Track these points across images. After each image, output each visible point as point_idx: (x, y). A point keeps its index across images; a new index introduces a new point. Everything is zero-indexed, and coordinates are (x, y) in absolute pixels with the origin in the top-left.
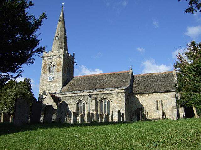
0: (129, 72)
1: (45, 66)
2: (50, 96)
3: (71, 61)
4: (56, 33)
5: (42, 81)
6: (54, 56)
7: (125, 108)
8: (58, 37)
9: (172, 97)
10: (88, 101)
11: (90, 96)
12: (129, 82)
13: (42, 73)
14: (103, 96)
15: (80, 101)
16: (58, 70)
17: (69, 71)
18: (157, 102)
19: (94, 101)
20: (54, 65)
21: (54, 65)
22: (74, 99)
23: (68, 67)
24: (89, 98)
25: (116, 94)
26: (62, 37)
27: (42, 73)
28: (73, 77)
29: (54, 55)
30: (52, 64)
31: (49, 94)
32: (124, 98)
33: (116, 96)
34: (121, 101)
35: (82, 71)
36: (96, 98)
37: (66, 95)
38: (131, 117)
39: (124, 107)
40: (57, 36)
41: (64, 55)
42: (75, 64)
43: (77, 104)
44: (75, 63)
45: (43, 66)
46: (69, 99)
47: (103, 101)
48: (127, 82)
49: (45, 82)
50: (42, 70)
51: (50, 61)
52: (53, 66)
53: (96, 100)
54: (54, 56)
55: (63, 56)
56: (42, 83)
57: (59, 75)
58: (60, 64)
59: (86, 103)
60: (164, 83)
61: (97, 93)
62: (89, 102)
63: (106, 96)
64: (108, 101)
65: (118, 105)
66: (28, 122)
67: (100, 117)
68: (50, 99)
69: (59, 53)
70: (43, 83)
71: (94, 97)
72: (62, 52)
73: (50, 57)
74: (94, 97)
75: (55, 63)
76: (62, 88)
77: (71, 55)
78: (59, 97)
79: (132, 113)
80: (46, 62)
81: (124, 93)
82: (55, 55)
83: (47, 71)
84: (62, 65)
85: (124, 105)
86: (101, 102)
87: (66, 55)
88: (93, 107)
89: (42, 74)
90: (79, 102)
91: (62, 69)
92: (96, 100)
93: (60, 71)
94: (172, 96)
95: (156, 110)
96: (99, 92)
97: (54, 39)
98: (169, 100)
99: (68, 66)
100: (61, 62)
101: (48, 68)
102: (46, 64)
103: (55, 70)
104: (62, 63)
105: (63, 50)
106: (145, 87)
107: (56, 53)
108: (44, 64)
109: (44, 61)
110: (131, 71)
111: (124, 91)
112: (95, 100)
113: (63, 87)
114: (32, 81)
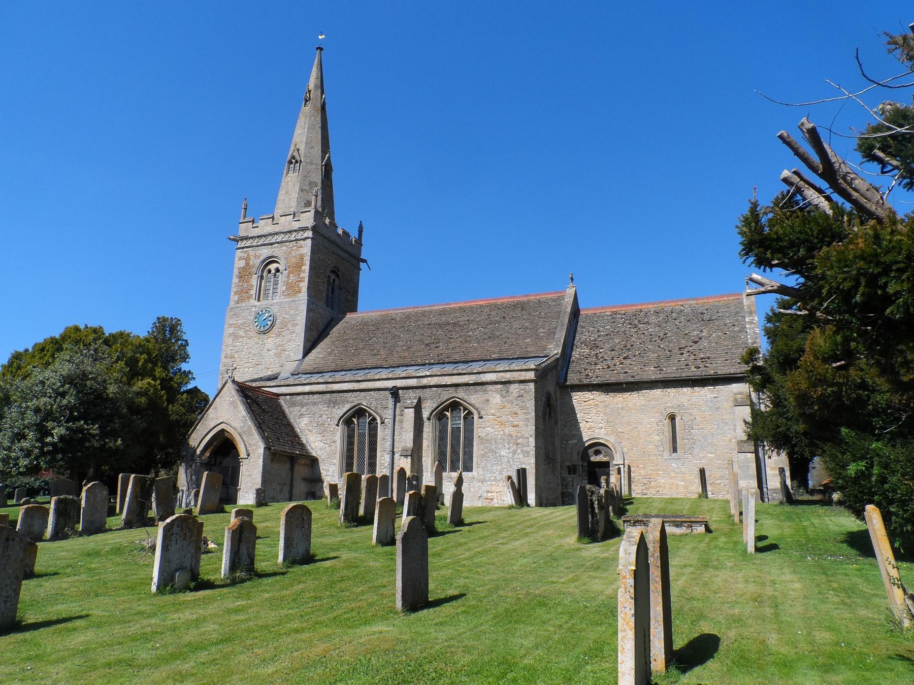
0: (563, 298)
1: (244, 274)
2: (234, 393)
3: (344, 255)
4: (292, 148)
5: (231, 330)
6: (276, 234)
7: (537, 447)
8: (297, 162)
9: (738, 404)
10: (388, 414)
11: (395, 393)
12: (561, 335)
13: (234, 298)
14: (446, 395)
15: (359, 412)
16: (292, 289)
17: (336, 292)
18: (672, 418)
19: (410, 413)
20: (278, 270)
21: (278, 270)
22: (335, 403)
23: (333, 277)
24: (391, 402)
25: (499, 386)
26: (311, 163)
27: (234, 298)
28: (354, 309)
29: (277, 230)
30: (273, 267)
31: (230, 385)
32: (531, 405)
33: (498, 396)
34: (521, 416)
35: (376, 297)
36: (420, 400)
37: (307, 389)
38: (563, 479)
39: (532, 441)
40: (293, 157)
41: (314, 229)
42: (362, 265)
43: (347, 421)
44: (365, 261)
45: (236, 271)
46: (315, 404)
47: (448, 414)
48: (551, 334)
49: (241, 333)
50: (234, 289)
51: (265, 252)
52: (273, 271)
53: (418, 409)
54: (276, 234)
55: (310, 234)
56: (230, 335)
57: (292, 306)
58: (299, 266)
59: (379, 421)
60: (704, 343)
61: (425, 381)
62: (391, 417)
63: (461, 394)
64: (469, 416)
65: (507, 431)
66: (827, 216)
67: (377, 512)
68: (232, 403)
69: (296, 225)
70: (236, 337)
71: (410, 398)
72: (308, 219)
73: (294, 234)
74: (410, 398)
75: (282, 261)
76: (304, 357)
77: (344, 232)
78: (278, 395)
79: (568, 463)
80: (247, 259)
81: (532, 386)
82: (282, 230)
83: (253, 292)
84: (306, 267)
85: (533, 432)
86: (440, 416)
87: (324, 231)
88: (406, 438)
89: (232, 304)
90: (353, 416)
91: (304, 285)
92: (418, 409)
93: (299, 292)
94: (736, 400)
95: (666, 455)
96: (432, 376)
97: (285, 172)
98: (722, 416)
99: (333, 272)
100: (302, 257)
101: (254, 280)
102: (247, 264)
103: (281, 287)
104: (308, 263)
105: (313, 212)
106: (625, 358)
107: (286, 223)
108: (242, 263)
109: (243, 254)
110: (570, 292)
111: (531, 375)
112: (416, 412)
113: (306, 353)
114: (188, 332)
